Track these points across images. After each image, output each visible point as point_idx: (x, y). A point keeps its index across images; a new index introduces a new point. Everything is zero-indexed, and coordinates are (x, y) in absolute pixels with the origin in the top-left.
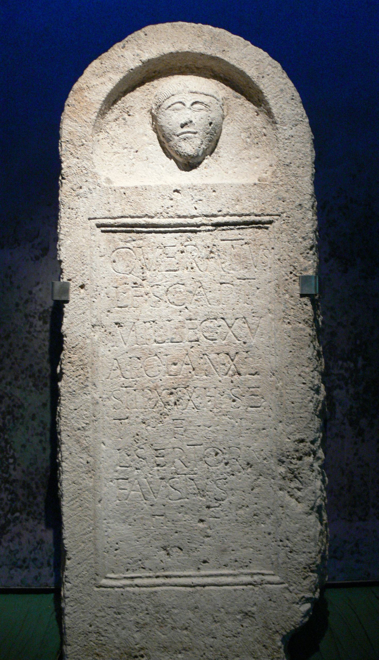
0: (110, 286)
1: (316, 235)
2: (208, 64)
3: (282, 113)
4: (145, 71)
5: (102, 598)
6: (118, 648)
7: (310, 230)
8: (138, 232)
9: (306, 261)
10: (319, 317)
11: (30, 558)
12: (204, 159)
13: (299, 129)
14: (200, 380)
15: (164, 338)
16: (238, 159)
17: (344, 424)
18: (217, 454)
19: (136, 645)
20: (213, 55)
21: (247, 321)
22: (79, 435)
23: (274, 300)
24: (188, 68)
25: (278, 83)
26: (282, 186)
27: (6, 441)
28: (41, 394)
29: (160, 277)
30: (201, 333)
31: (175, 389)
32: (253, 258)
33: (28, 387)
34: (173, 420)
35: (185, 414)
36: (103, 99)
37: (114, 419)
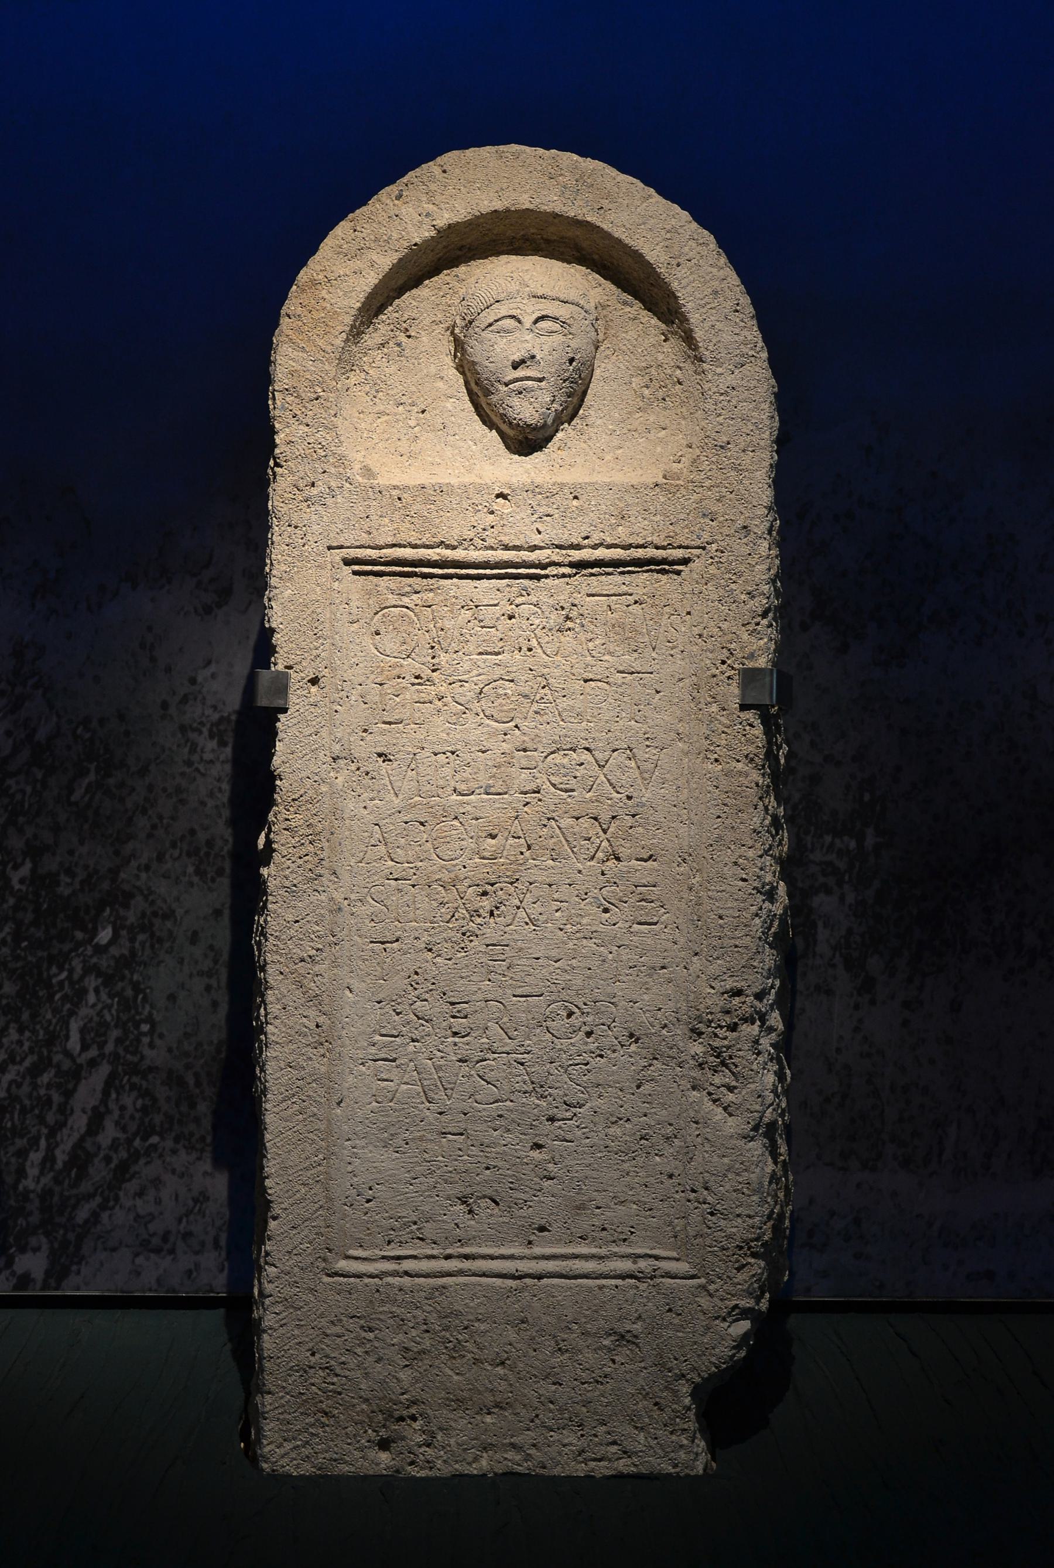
0: (368, 682)
1: (775, 587)
2: (569, 234)
3: (714, 341)
4: (440, 246)
5: (338, 1297)
6: (366, 1400)
7: (764, 577)
8: (425, 576)
9: (753, 640)
10: (779, 747)
11: (179, 1232)
12: (557, 431)
13: (748, 373)
14: (539, 869)
15: (473, 785)
16: (625, 431)
17: (834, 966)
18: (570, 1015)
19: (403, 1394)
20: (580, 218)
21: (634, 756)
22: (302, 971)
23: (689, 715)
24: (527, 240)
25: (708, 278)
26: (709, 489)
27: (136, 987)
28: (210, 890)
29: (467, 666)
30: (545, 777)
31: (492, 885)
32: (648, 633)
33: (185, 876)
34: (487, 945)
35: (511, 934)
36: (359, 305)
37: (372, 942)
